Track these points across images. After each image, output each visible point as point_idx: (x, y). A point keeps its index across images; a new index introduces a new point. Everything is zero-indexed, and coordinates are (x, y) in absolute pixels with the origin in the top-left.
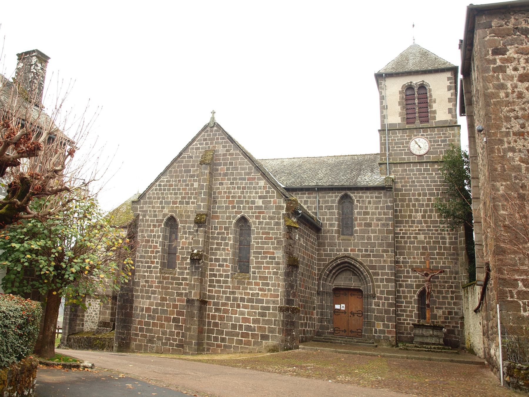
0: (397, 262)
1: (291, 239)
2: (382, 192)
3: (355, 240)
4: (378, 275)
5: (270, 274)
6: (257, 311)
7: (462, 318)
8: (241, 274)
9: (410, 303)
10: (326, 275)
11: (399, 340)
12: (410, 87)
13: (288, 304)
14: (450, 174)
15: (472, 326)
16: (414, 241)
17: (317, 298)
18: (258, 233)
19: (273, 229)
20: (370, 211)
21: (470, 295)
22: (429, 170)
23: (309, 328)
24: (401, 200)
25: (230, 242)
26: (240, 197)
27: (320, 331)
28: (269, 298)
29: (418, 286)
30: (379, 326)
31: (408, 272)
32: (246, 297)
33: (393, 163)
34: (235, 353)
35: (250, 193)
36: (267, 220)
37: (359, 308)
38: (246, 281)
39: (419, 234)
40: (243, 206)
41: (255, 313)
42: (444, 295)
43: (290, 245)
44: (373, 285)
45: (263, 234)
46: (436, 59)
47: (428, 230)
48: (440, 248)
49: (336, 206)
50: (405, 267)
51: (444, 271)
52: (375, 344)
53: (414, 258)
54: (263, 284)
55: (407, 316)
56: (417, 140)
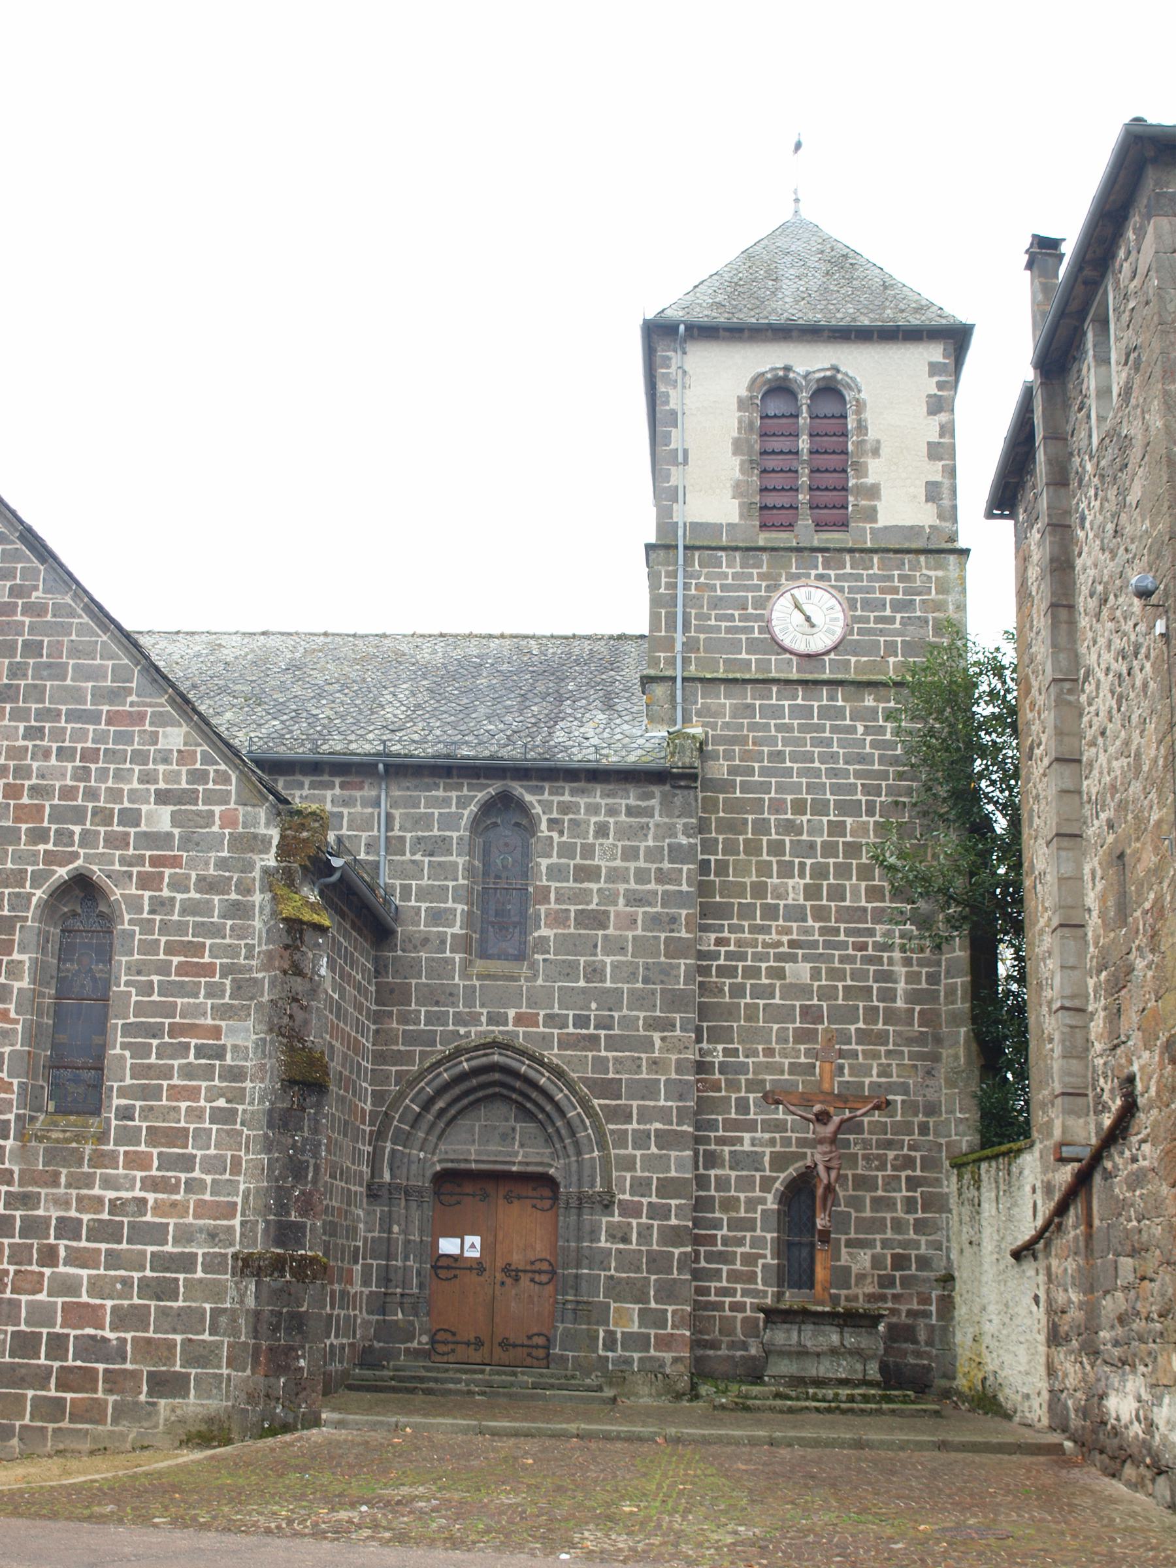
0: (701, 1067)
1: (298, 971)
2: (656, 790)
3: (535, 977)
4: (628, 1118)
5: (200, 1118)
6: (136, 1275)
7: (948, 1279)
8: (62, 1121)
9: (750, 1225)
10: (410, 1118)
11: (701, 1371)
12: (779, 387)
13: (279, 1243)
14: (931, 732)
15: (991, 1308)
16: (772, 986)
17: (368, 1213)
18: (150, 947)
19: (216, 931)
20: (604, 865)
21: (988, 1194)
22: (839, 713)
23: (337, 1337)
24: (724, 826)
25: (17, 985)
26: (68, 793)
27: (377, 1345)
28: (190, 1219)
29: (780, 1162)
30: (627, 1319)
31: (743, 1106)
32: (86, 1217)
33: (702, 680)
34: (27, 1456)
35: (119, 776)
36: (193, 894)
37: (540, 1249)
38: (88, 1149)
39: (793, 958)
40: (84, 833)
41: (127, 1282)
42: (880, 1193)
43: (295, 1000)
44: (606, 1161)
45: (171, 949)
46: (885, 287)
47: (828, 945)
48: (871, 1013)
49: (460, 838)
50: (733, 1086)
51: (888, 1103)
52: (609, 1393)
53: (769, 1052)
54: (166, 1162)
55: (734, 1276)
56: (800, 594)
